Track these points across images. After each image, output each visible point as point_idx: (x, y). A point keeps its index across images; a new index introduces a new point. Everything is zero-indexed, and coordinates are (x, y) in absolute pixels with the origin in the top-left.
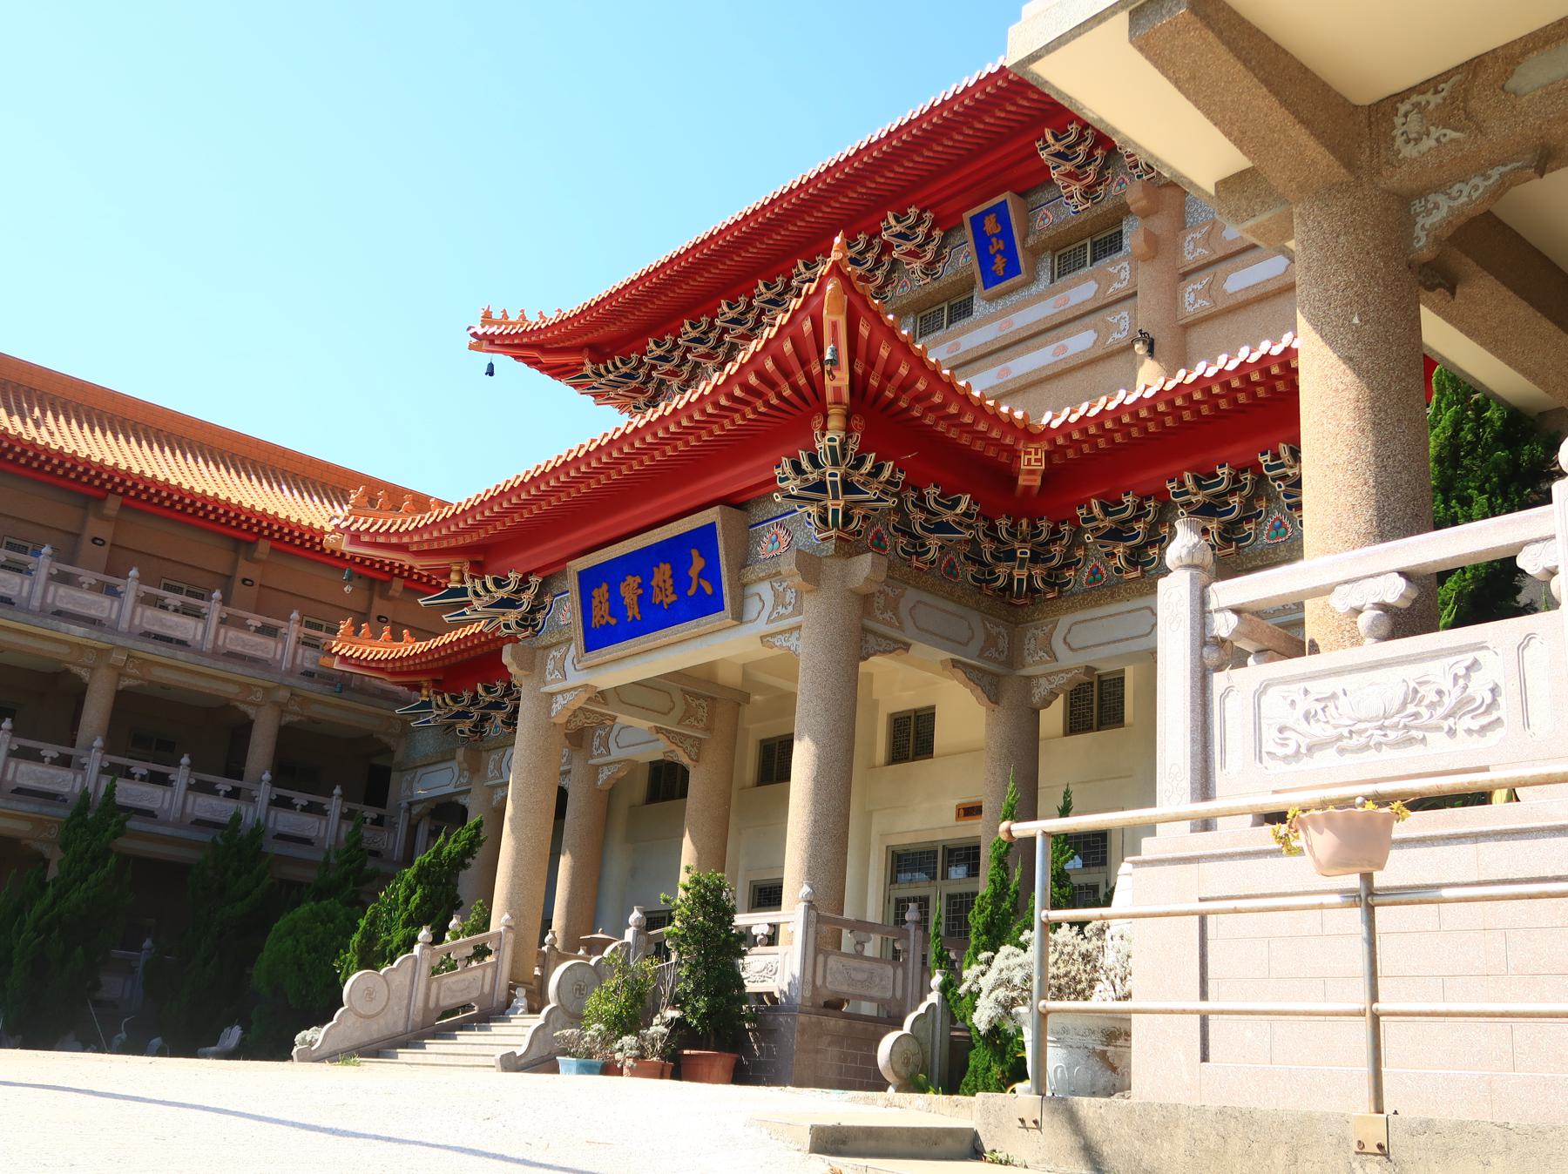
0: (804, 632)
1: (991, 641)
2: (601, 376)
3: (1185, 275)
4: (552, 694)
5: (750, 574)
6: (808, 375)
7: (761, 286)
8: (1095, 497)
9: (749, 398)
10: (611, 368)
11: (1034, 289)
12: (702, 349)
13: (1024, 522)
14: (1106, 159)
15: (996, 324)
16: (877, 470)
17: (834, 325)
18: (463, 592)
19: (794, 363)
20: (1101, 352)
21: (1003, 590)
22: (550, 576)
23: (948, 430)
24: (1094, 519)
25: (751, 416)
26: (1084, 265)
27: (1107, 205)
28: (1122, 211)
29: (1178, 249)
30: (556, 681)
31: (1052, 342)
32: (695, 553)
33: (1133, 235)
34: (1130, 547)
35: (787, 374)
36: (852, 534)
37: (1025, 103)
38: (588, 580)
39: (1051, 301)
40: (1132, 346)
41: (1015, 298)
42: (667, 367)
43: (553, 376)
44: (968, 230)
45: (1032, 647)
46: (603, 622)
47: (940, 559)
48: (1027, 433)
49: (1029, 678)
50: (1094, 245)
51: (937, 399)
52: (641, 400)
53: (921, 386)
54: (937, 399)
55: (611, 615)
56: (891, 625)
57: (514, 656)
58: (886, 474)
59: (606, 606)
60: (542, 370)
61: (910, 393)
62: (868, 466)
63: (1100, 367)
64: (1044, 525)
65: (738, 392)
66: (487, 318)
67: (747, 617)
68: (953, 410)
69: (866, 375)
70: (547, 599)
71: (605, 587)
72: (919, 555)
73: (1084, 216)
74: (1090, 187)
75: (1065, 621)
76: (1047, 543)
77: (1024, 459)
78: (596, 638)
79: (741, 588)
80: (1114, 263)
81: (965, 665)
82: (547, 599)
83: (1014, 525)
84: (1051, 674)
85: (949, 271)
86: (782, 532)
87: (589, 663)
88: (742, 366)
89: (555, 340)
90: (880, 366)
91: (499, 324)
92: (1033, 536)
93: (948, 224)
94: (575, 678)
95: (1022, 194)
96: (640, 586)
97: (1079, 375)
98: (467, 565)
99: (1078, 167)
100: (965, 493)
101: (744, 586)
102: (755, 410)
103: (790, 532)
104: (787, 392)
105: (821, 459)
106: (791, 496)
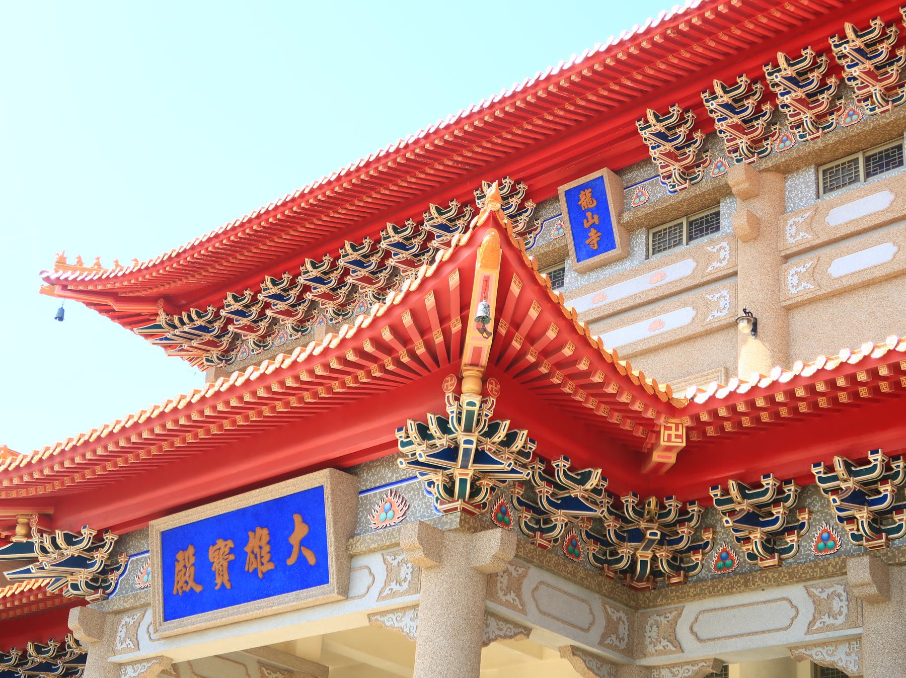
0: (421, 612)
1: (611, 627)
2: (175, 327)
3: (787, 258)
4: (121, 665)
5: (359, 545)
6: (446, 333)
7: (348, 248)
8: (732, 477)
9: (379, 354)
10: (185, 319)
11: (628, 264)
12: (282, 306)
13: (653, 500)
14: (705, 141)
15: (590, 296)
16: (510, 438)
17: (487, 280)
18: (29, 547)
19: (434, 319)
20: (699, 329)
21: (623, 572)
22: (127, 533)
23: (587, 401)
24: (731, 501)
25: (377, 374)
26: (680, 243)
27: (705, 186)
28: (725, 191)
29: (779, 233)
30: (128, 650)
31: (648, 317)
32: (297, 518)
33: (732, 216)
34: (767, 533)
35: (423, 331)
36: (477, 506)
37: (629, 83)
38: (172, 542)
39: (648, 276)
40: (736, 323)
41: (608, 272)
42: (244, 321)
43: (124, 324)
44: (563, 205)
45: (654, 634)
46: (187, 589)
47: (564, 537)
48: (671, 408)
49: (649, 668)
50: (690, 224)
51: (583, 366)
52: (215, 353)
53: (567, 351)
54: (583, 366)
55: (197, 580)
56: (514, 608)
57: (82, 621)
58: (519, 444)
59: (191, 571)
60: (113, 318)
61: (554, 358)
62: (501, 434)
63: (700, 344)
64: (673, 504)
65: (368, 348)
66: (61, 263)
67: (351, 594)
68: (597, 378)
69: (509, 337)
70: (122, 560)
71: (191, 550)
72: (543, 531)
73: (682, 196)
74: (687, 168)
75: (691, 608)
76: (674, 525)
77: (664, 434)
78: (177, 606)
79: (349, 557)
80: (712, 242)
81: (591, 655)
82: (122, 560)
83: (641, 503)
84: (674, 665)
85: (541, 242)
86: (396, 501)
87: (168, 633)
88: (376, 319)
89: (131, 288)
90: (526, 327)
91: (74, 269)
92: (661, 516)
93: (541, 197)
94: (149, 648)
95: (618, 172)
96: (232, 551)
97: (676, 351)
98: (35, 519)
99: (677, 149)
100: (595, 467)
101: (352, 557)
102: (382, 368)
103: (406, 501)
104: (421, 350)
105: (452, 424)
106: (417, 463)
